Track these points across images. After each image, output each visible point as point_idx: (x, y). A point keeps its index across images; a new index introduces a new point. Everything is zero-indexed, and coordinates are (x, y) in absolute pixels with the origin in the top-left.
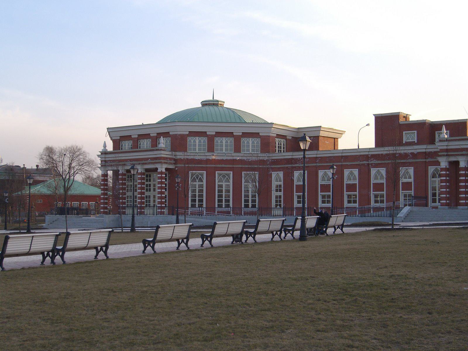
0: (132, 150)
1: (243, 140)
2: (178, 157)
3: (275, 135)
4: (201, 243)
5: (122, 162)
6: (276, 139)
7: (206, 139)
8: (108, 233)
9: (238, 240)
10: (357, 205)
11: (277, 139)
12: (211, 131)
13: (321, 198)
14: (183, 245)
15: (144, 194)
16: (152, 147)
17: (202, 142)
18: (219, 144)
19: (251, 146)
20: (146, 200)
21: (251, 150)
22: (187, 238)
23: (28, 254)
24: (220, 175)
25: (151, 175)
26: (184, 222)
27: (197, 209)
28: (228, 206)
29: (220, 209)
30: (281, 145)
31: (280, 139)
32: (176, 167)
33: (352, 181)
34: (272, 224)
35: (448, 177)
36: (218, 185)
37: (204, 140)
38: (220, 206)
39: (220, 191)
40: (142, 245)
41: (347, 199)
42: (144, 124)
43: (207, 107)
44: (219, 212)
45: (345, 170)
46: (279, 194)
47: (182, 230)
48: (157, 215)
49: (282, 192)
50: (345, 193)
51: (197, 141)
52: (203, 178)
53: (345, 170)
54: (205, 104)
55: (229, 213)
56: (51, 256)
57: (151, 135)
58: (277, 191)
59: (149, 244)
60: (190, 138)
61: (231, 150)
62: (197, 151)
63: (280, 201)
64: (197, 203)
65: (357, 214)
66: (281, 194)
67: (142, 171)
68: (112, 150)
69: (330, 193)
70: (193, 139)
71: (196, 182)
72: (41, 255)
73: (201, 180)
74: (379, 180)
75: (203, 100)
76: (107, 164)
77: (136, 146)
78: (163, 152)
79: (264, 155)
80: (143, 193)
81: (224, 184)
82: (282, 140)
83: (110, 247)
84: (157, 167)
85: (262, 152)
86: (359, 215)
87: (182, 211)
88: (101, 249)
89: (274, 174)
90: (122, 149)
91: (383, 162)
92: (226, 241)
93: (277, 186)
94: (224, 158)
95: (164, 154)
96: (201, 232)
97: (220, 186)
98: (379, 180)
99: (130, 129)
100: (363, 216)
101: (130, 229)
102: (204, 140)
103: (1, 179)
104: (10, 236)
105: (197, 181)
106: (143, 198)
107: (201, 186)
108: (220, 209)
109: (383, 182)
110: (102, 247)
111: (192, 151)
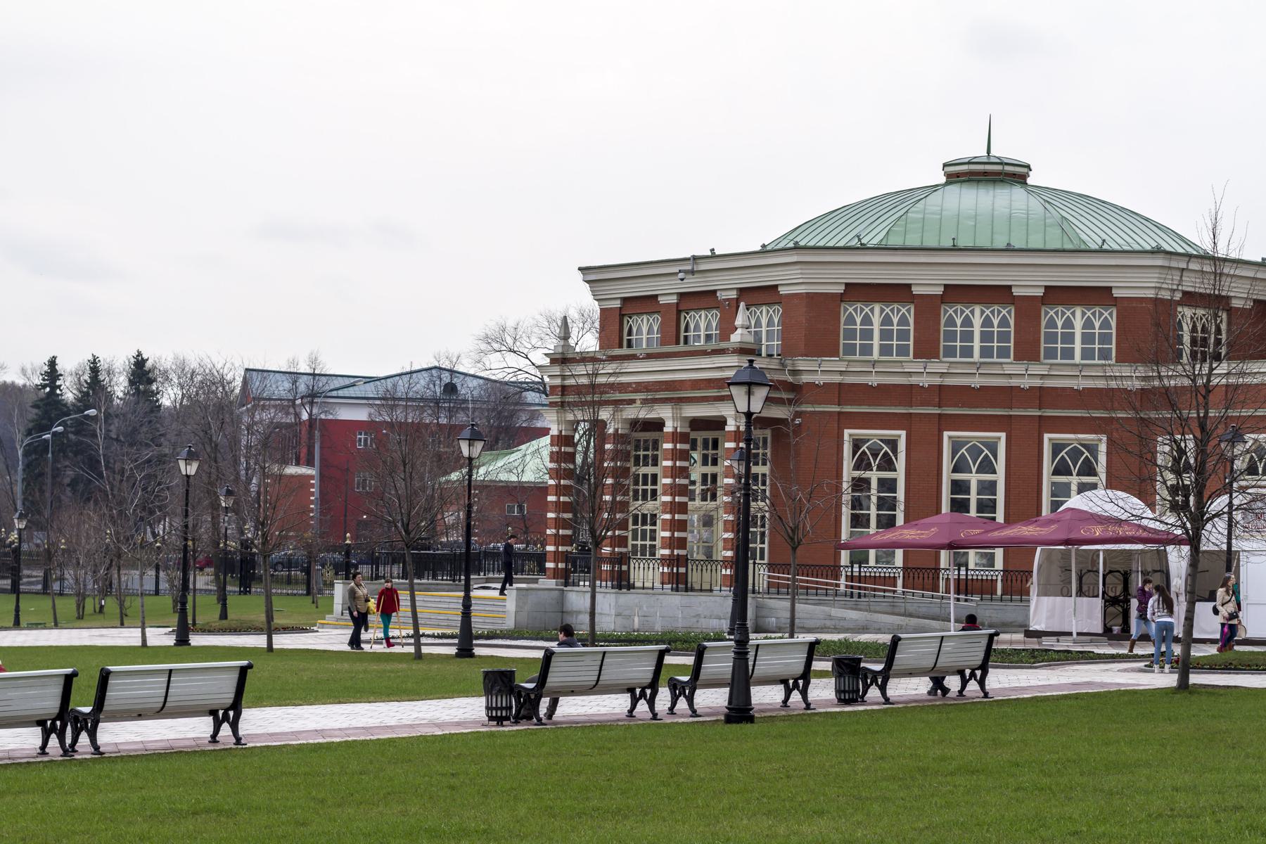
1: (1047, 313)
5: (613, 395)
7: (1009, 313)
9: (847, 698)
11: (1188, 312)
16: (663, 342)
17: (1060, 326)
18: (895, 328)
20: (633, 530)
22: (984, 668)
23: (162, 711)
25: (717, 439)
35: (606, 501)
36: (1053, 484)
37: (903, 314)
42: (717, 252)
51: (1078, 323)
52: (896, 459)
56: (978, 678)
57: (722, 296)
59: (874, 681)
60: (951, 311)
65: (999, 592)
67: (738, 427)
70: (1101, 314)
71: (971, 473)
72: (782, 686)
73: (987, 467)
76: (570, 398)
77: (674, 334)
79: (1126, 370)
81: (974, 478)
83: (247, 714)
84: (661, 415)
87: (779, 578)
88: (973, 675)
90: (686, 342)
91: (808, 409)
94: (1023, 383)
97: (959, 487)
101: (456, 641)
103: (1264, 435)
105: (974, 470)
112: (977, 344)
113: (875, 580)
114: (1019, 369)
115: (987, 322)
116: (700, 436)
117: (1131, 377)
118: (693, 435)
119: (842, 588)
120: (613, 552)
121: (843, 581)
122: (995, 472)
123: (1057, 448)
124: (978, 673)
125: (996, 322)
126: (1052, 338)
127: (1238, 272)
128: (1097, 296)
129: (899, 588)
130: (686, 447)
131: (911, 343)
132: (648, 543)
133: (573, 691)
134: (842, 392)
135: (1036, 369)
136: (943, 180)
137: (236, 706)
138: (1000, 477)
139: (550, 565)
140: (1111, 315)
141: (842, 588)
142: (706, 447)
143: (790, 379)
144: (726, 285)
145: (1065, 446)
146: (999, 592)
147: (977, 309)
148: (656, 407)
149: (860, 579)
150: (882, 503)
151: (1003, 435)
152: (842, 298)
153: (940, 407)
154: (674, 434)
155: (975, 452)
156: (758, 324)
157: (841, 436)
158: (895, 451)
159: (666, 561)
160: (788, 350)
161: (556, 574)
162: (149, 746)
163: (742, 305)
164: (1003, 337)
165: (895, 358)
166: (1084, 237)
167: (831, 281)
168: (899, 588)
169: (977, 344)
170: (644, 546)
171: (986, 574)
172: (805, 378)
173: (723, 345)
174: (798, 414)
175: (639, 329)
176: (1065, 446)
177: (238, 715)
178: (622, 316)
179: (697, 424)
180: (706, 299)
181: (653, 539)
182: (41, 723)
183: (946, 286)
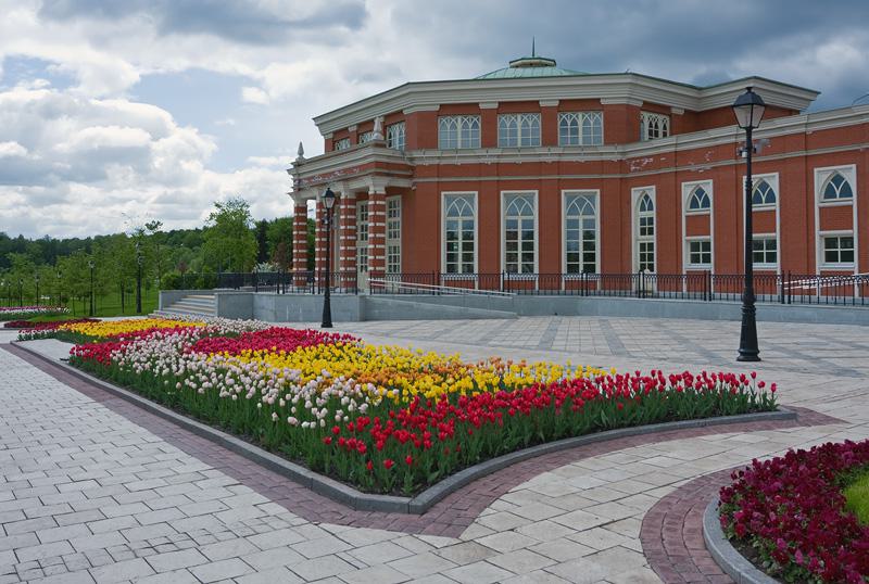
3: (640, 104)
6: (642, 112)
10: (854, 266)
11: (646, 116)
15: (384, 244)
19: (519, 133)
24: (570, 198)
26: (135, 309)
27: (580, 276)
28: (469, 269)
29: (451, 277)
30: (656, 126)
31: (654, 115)
32: (414, 184)
33: (764, 204)
37: (534, 121)
38: (451, 269)
39: (512, 235)
41: (690, 253)
44: (570, 284)
46: (647, 239)
48: (792, 304)
49: (654, 236)
50: (684, 238)
51: (580, 122)
57: (674, 111)
58: (643, 232)
62: (581, 143)
63: (651, 257)
64: (520, 263)
65: (563, 288)
66: (653, 239)
68: (323, 153)
69: (708, 237)
73: (467, 212)
74: (838, 199)
79: (610, 149)
80: (382, 241)
82: (661, 117)
85: (607, 142)
86: (569, 291)
89: (636, 194)
93: (643, 221)
98: (838, 199)
99: (373, 103)
100: (708, 297)
102: (534, 121)
106: (382, 252)
107: (469, 225)
108: (451, 277)
109: (773, 208)
114: (545, 151)
117: (613, 153)
120: (375, 270)
122: (472, 215)
127: (639, 82)
128: (591, 105)
134: (440, 170)
135: (554, 150)
138: (597, 217)
140: (600, 117)
143: (409, 163)
146: (563, 288)
151: (476, 193)
153: (498, 175)
154: (346, 199)
155: (581, 202)
157: (560, 195)
160: (409, 147)
167: (431, 104)
171: (469, 277)
172: (417, 163)
174: (414, 184)
178: (358, 135)
183: (500, 103)
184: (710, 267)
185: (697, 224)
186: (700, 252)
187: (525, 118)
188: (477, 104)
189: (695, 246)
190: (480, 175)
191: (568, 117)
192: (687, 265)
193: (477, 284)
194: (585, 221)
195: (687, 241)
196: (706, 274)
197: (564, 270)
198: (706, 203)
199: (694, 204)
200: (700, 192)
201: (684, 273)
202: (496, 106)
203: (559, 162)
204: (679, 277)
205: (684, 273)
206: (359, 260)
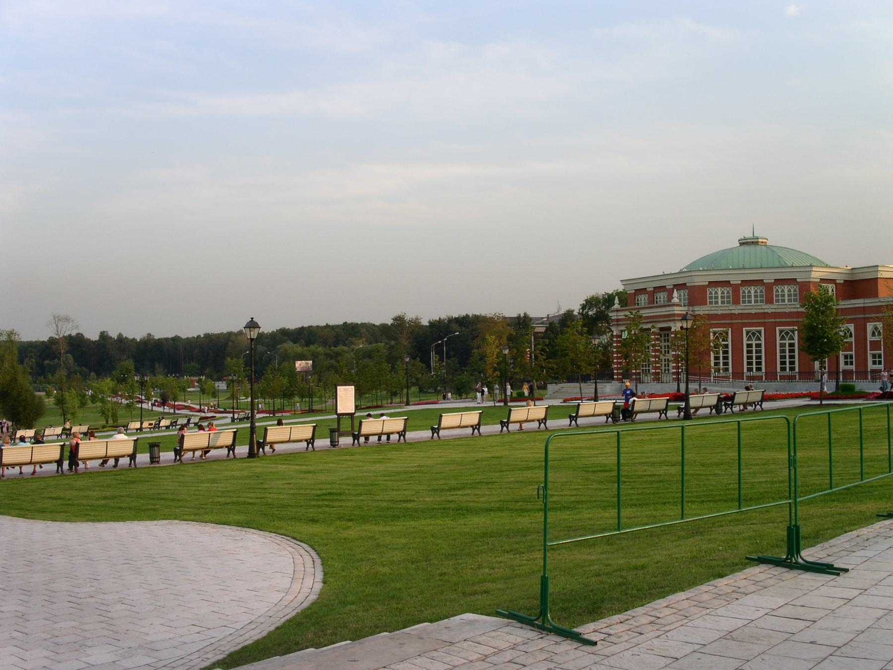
0: (650, 306)
1: (742, 289)
2: (697, 313)
4: (710, 411)
7: (730, 289)
8: (233, 433)
12: (736, 280)
13: (843, 358)
14: (663, 415)
16: (649, 303)
21: (786, 300)
34: (652, 403)
40: (499, 426)
43: (747, 248)
45: (868, 324)
47: (537, 410)
50: (869, 352)
51: (753, 292)
53: (868, 324)
54: (744, 243)
55: (727, 377)
59: (729, 407)
61: (728, 302)
75: (740, 239)
78: (676, 308)
81: (754, 343)
82: (830, 285)
83: (482, 427)
88: (758, 404)
90: (638, 304)
92: (780, 403)
95: (678, 310)
96: (415, 426)
104: (268, 428)
107: (791, 345)
108: (783, 373)
110: (476, 426)
111: (780, 303)
112: (753, 299)
113: (723, 377)
115: (789, 291)
116: (663, 333)
118: (661, 333)
119: (712, 380)
121: (712, 378)
123: (781, 332)
124: (760, 403)
125: (759, 292)
126: (711, 298)
129: (731, 380)
130: (659, 337)
131: (708, 300)
132: (647, 368)
133: (642, 412)
136: (739, 245)
137: (313, 438)
139: (615, 377)
140: (797, 287)
141: (712, 380)
142: (665, 336)
144: (669, 284)
145: (750, 332)
147: (752, 288)
148: (668, 323)
149: (718, 377)
150: (757, 352)
152: (707, 286)
156: (680, 296)
158: (728, 335)
159: (674, 373)
161: (618, 379)
162: (416, 439)
163: (675, 290)
164: (728, 297)
165: (726, 305)
166: (787, 262)
168: (731, 380)
169: (753, 299)
170: (646, 370)
171: (759, 374)
173: (669, 303)
175: (641, 299)
176: (750, 332)
177: (313, 441)
179: (661, 329)
180: (662, 288)
181: (668, 366)
182: (128, 456)
183: (742, 281)
184: (853, 367)
185: (875, 345)
186: (876, 359)
187: (789, 287)
188: (729, 281)
189: (874, 356)
190: (732, 320)
191: (779, 288)
192: (871, 366)
193: (797, 377)
194: (756, 344)
195: (871, 354)
196: (851, 372)
197: (779, 370)
198: (851, 336)
199: (873, 334)
200: (876, 328)
201: (869, 370)
202: (740, 282)
203: (864, 307)
204: (866, 372)
205: (869, 370)
206: (663, 365)
